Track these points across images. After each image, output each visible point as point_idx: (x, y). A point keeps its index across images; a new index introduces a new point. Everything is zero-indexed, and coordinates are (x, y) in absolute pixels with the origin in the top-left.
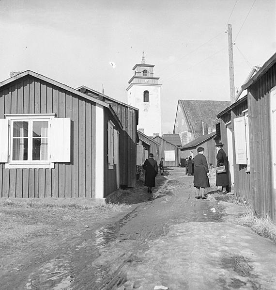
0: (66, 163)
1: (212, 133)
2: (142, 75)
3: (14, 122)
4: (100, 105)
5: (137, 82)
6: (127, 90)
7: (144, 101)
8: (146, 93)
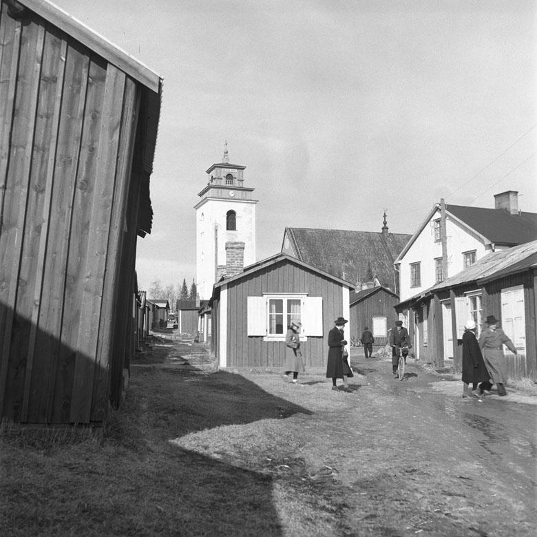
0: (317, 337)
1: (362, 292)
2: (223, 183)
3: (270, 300)
4: (346, 286)
5: (215, 196)
6: (197, 207)
7: (227, 229)
8: (231, 215)
